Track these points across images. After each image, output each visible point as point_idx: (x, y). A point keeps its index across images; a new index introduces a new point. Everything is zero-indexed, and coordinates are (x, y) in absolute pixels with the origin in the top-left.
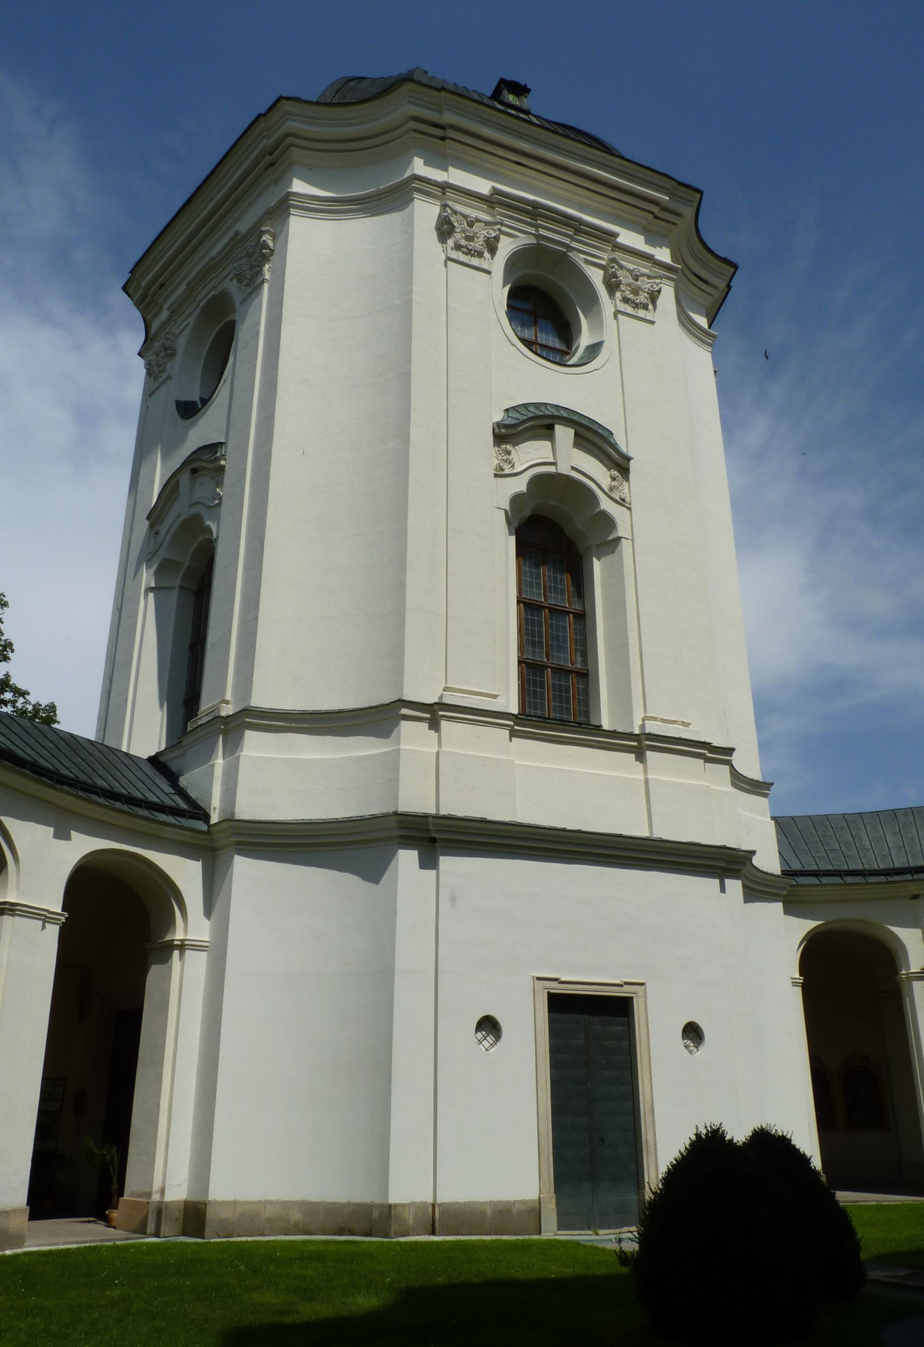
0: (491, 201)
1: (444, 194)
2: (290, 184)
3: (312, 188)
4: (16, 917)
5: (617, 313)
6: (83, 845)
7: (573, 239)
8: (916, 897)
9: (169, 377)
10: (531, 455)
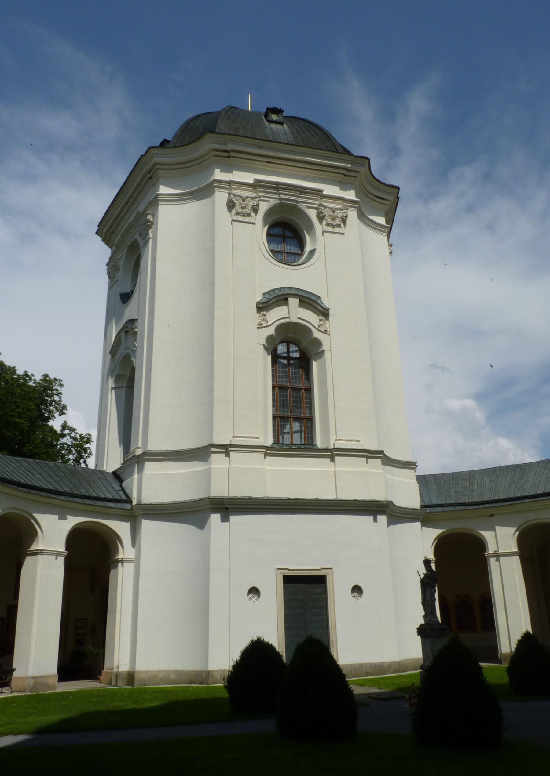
0: (256, 185)
1: (230, 186)
2: (158, 189)
3: (171, 189)
4: (44, 556)
5: (323, 232)
6: (73, 521)
7: (299, 197)
8: (492, 515)
9: (117, 281)
10: (278, 315)
